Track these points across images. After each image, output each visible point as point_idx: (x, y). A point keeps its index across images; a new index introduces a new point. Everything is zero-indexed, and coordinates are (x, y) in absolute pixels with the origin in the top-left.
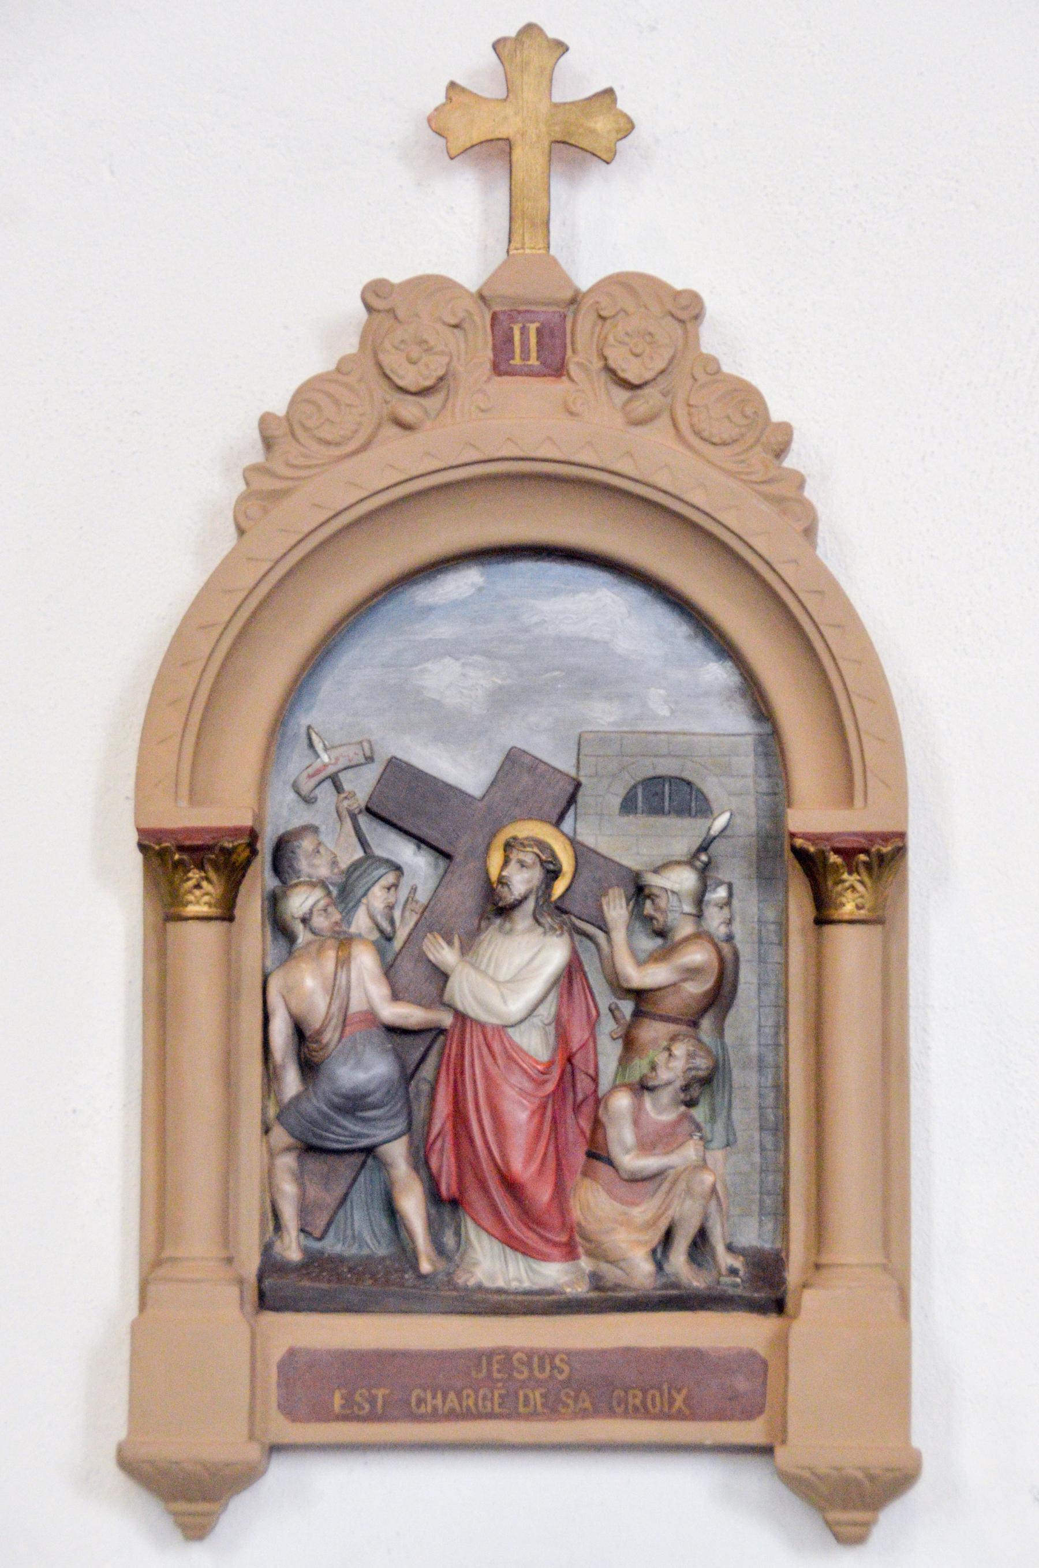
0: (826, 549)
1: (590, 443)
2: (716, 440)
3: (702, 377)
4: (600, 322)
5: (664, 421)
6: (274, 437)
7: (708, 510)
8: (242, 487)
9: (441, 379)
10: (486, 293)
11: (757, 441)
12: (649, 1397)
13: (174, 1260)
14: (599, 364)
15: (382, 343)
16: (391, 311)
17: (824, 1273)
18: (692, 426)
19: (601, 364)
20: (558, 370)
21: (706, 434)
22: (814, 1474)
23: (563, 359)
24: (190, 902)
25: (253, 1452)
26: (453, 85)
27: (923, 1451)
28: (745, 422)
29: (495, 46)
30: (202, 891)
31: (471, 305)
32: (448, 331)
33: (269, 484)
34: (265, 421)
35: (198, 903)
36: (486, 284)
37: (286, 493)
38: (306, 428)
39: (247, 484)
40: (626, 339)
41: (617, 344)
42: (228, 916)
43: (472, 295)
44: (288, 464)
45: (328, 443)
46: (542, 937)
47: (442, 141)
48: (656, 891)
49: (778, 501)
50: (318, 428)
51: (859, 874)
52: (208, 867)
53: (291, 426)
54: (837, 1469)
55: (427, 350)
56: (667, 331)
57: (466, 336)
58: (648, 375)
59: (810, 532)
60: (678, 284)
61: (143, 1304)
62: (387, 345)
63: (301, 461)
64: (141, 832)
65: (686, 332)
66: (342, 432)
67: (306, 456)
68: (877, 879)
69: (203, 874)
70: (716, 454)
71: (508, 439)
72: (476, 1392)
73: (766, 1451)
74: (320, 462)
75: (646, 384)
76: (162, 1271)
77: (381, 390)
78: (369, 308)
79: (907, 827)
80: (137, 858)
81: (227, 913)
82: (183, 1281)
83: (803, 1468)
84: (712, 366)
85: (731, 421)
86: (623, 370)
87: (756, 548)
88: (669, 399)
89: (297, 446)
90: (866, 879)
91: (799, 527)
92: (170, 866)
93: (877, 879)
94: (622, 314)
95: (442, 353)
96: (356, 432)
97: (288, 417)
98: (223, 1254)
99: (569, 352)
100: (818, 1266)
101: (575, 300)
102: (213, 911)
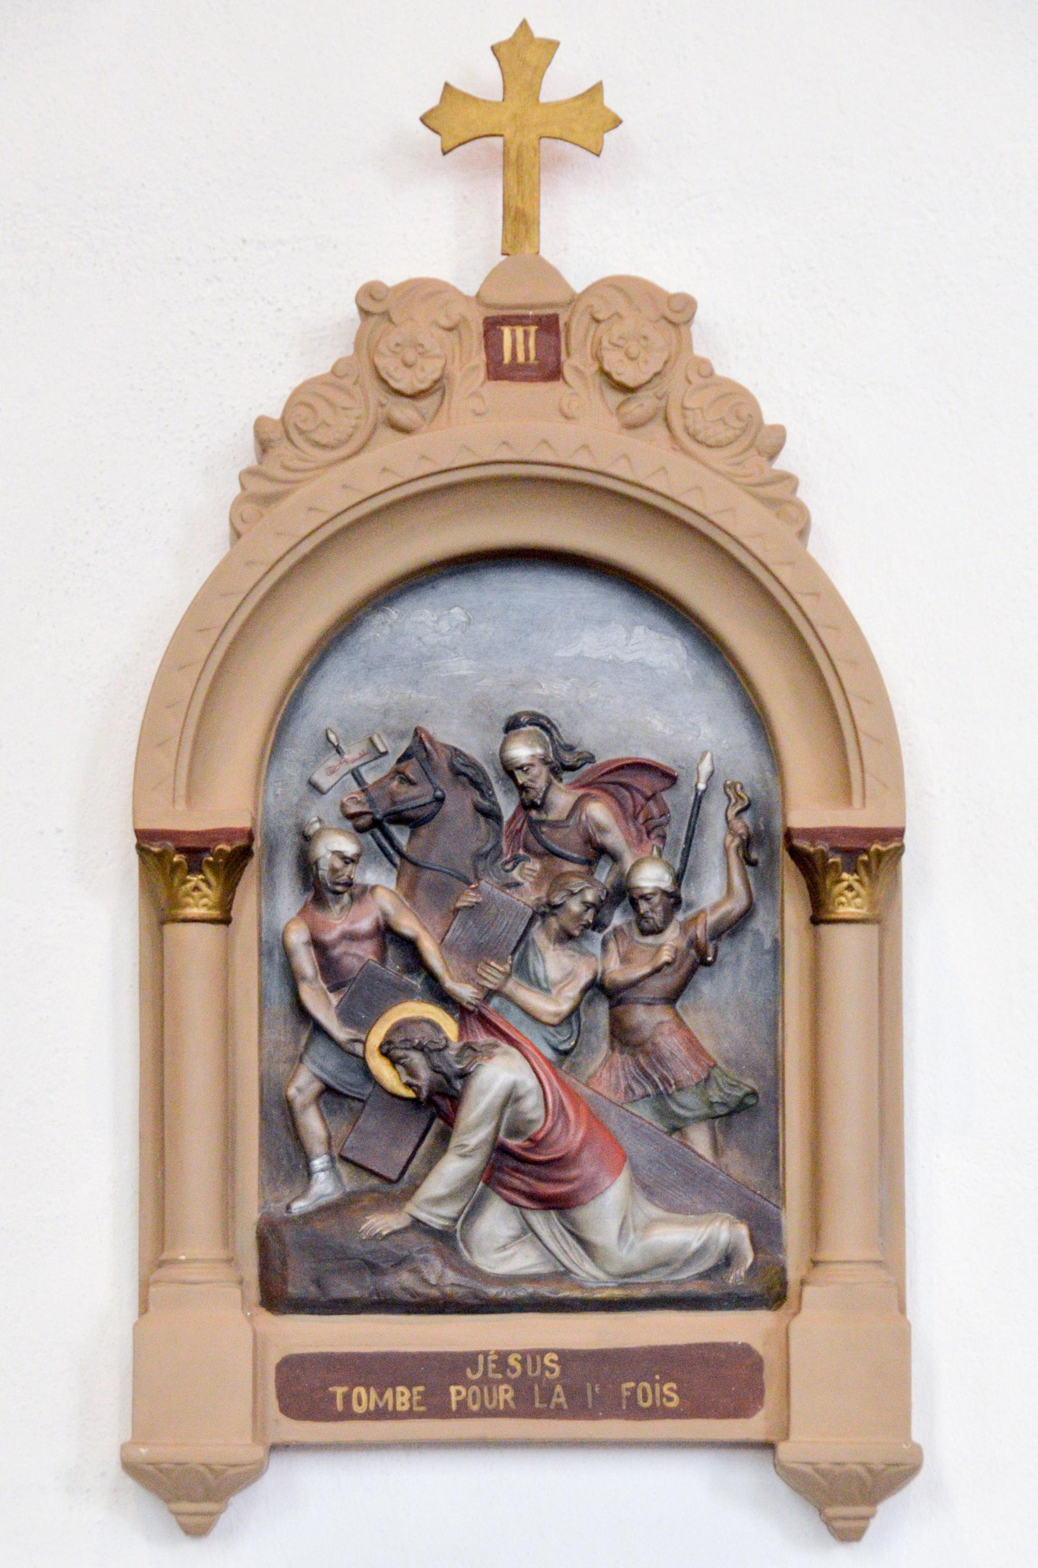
0: (814, 547)
2: (711, 441)
4: (594, 325)
6: (270, 441)
8: (237, 490)
11: (751, 445)
15: (378, 343)
16: (386, 315)
17: (821, 1270)
18: (686, 429)
19: (596, 367)
21: (700, 437)
22: (817, 1470)
23: (558, 360)
24: (188, 905)
25: (258, 1452)
27: (923, 1446)
28: (739, 424)
33: (266, 487)
34: (260, 424)
38: (302, 432)
39: (243, 487)
40: (621, 342)
41: (610, 347)
42: (226, 921)
43: (467, 298)
45: (324, 446)
49: (771, 503)
51: (858, 874)
57: (460, 337)
59: (803, 534)
60: (672, 288)
62: (382, 347)
66: (337, 436)
68: (874, 878)
70: (715, 457)
73: (769, 1446)
77: (376, 393)
78: (365, 313)
79: (905, 822)
80: (134, 857)
82: (184, 1282)
84: (705, 370)
87: (339, 510)
88: (664, 401)
89: (296, 451)
90: (866, 879)
91: (796, 529)
93: (874, 878)
94: (615, 318)
95: (438, 357)
97: (283, 419)
98: (222, 1254)
99: (563, 357)
100: (815, 1263)
102: (215, 913)
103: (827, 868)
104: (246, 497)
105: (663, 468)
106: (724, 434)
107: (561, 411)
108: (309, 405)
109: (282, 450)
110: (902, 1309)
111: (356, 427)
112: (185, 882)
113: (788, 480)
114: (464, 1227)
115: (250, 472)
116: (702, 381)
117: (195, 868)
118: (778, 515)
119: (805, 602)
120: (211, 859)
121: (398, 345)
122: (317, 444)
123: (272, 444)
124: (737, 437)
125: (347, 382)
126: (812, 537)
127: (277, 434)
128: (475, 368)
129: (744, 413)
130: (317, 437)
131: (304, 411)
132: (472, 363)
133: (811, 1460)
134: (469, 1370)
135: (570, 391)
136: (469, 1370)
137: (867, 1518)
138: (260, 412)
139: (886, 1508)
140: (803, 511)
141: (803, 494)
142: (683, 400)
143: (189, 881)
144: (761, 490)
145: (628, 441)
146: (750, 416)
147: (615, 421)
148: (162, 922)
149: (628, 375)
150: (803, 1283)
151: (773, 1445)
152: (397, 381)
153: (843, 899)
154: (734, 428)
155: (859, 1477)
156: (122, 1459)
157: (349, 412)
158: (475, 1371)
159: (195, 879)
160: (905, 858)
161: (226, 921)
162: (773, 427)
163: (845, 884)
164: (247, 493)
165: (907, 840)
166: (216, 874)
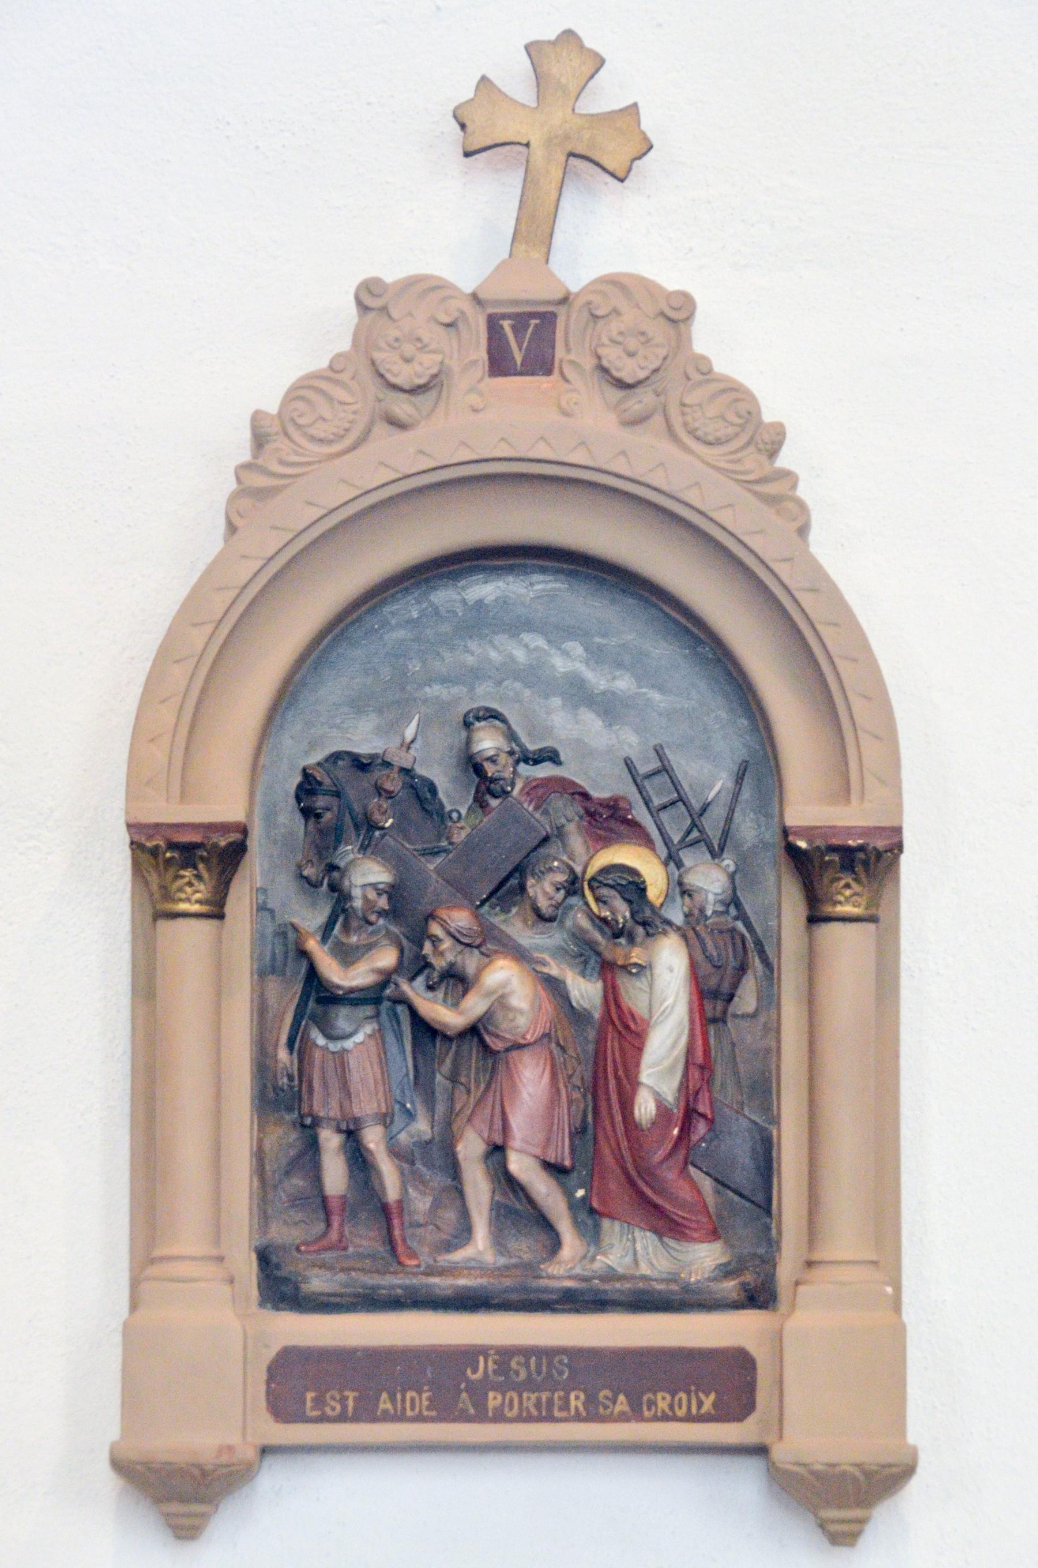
1: (623, 453)
3: (696, 377)
5: (658, 420)
6: (268, 435)
10: (481, 296)
12: (677, 1399)
16: (384, 310)
17: (817, 1273)
18: (685, 424)
30: (194, 888)
31: (467, 307)
32: (441, 330)
33: (259, 481)
34: (257, 419)
36: (480, 286)
38: (299, 427)
39: (239, 480)
40: (620, 339)
42: (220, 916)
44: (282, 462)
45: (321, 441)
46: (461, 152)
49: (772, 500)
53: (282, 422)
55: (420, 349)
56: (658, 331)
58: (642, 375)
59: (803, 531)
61: (134, 1305)
65: (679, 335)
67: (297, 453)
69: (195, 872)
71: (503, 439)
72: (673, 1396)
73: (761, 1451)
75: (639, 383)
77: (373, 387)
78: (363, 307)
81: (216, 912)
83: (798, 1464)
84: (703, 368)
86: (618, 370)
88: (662, 398)
89: (291, 444)
90: (863, 876)
91: (796, 525)
94: (614, 315)
97: (280, 414)
100: (810, 1264)
103: (825, 866)
106: (721, 430)
108: (302, 398)
111: (347, 430)
113: (788, 476)
114: (270, 1196)
115: (246, 467)
116: (702, 377)
117: (189, 863)
118: (778, 512)
119: (805, 599)
122: (313, 439)
124: (737, 435)
125: (345, 377)
126: (815, 536)
128: (474, 363)
129: (742, 407)
130: (312, 431)
131: (300, 405)
132: (473, 357)
134: (469, 1372)
136: (469, 1372)
140: (802, 507)
141: (803, 492)
143: (183, 877)
146: (749, 413)
149: (628, 370)
152: (396, 376)
154: (733, 425)
155: (855, 1479)
157: (346, 407)
158: (475, 1370)
160: (905, 860)
162: (772, 425)
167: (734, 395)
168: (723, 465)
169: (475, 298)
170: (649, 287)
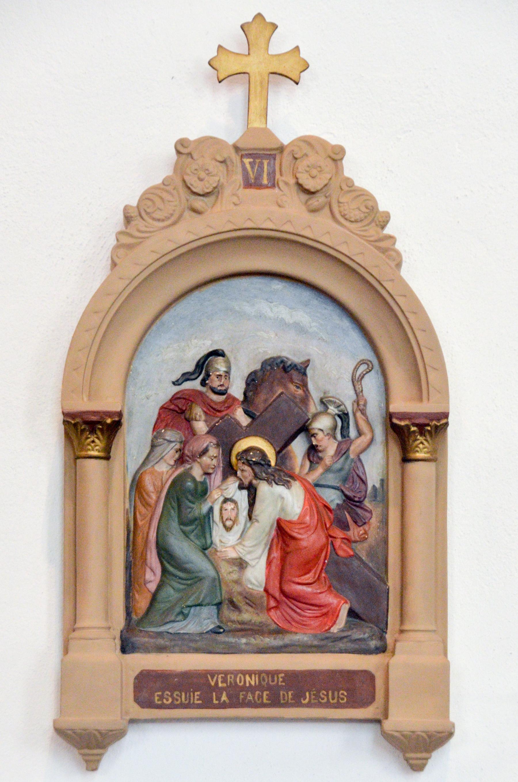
0: (405, 273)
4: (294, 161)
5: (326, 210)
6: (132, 217)
7: (349, 256)
8: (115, 242)
9: (215, 188)
11: (373, 220)
13: (79, 628)
14: (292, 181)
16: (190, 154)
18: (340, 212)
20: (273, 185)
22: (403, 735)
26: (220, 47)
28: (367, 211)
29: (242, 27)
31: (233, 151)
34: (126, 209)
35: (93, 450)
37: (141, 243)
38: (148, 213)
39: (117, 240)
44: (139, 231)
45: (159, 220)
47: (216, 72)
48: (316, 431)
49: (384, 251)
50: (153, 212)
51: (96, 434)
52: (427, 434)
54: (413, 732)
58: (319, 188)
59: (399, 265)
61: (66, 650)
63: (144, 229)
64: (65, 414)
73: (378, 721)
74: (155, 229)
76: (76, 634)
77: (183, 192)
78: (178, 152)
84: (349, 182)
85: (360, 210)
88: (329, 199)
89: (144, 222)
90: (429, 439)
91: (395, 263)
92: (79, 430)
96: (172, 215)
97: (138, 207)
99: (278, 176)
100: (402, 631)
101: (281, 149)
104: (119, 246)
105: (310, 226)
107: (277, 203)
109: (137, 222)
110: (445, 654)
112: (87, 438)
113: (391, 238)
117: (93, 431)
120: (101, 427)
121: (196, 170)
122: (154, 219)
123: (132, 219)
126: (404, 266)
127: (134, 213)
131: (149, 203)
133: (399, 730)
135: (282, 193)
136: (302, 699)
137: (427, 759)
138: (126, 203)
139: (435, 754)
140: (398, 254)
141: (398, 246)
142: (338, 198)
144: (377, 244)
145: (309, 217)
147: (304, 208)
148: (77, 458)
149: (310, 184)
150: (396, 641)
151: (380, 721)
153: (90, 447)
156: (54, 727)
159: (93, 438)
161: (107, 458)
162: (383, 212)
163: (419, 442)
164: (119, 243)
165: (450, 419)
166: (102, 434)
167: (365, 198)
168: (358, 232)
169: (236, 148)
170: (323, 143)
